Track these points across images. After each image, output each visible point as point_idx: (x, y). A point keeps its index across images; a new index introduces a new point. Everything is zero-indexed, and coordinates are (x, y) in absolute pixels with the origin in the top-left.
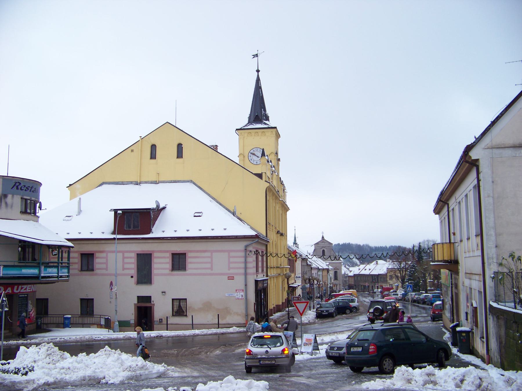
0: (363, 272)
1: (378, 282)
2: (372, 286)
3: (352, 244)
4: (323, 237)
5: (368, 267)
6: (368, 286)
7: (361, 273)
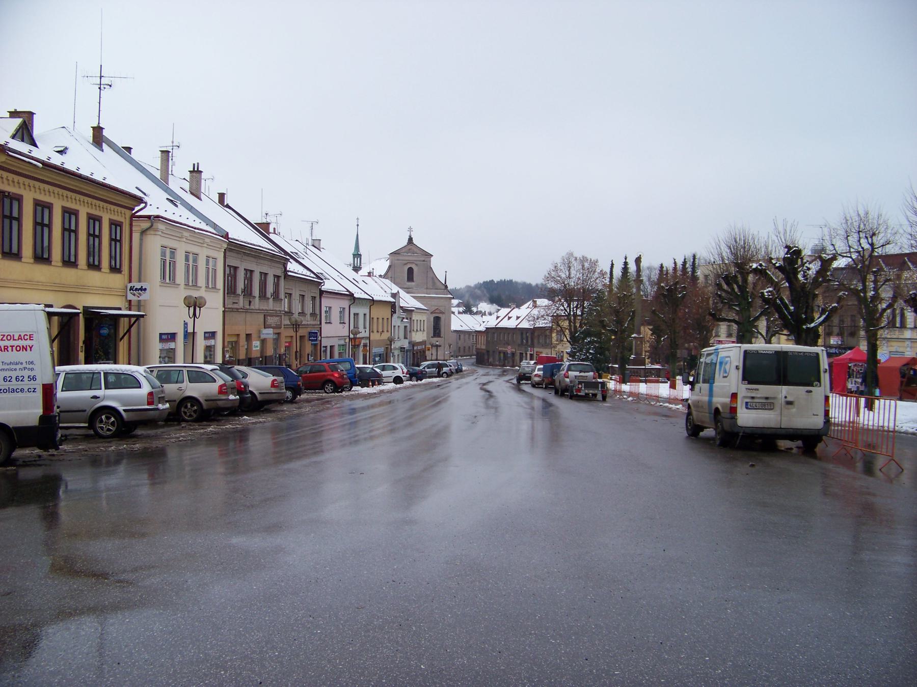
0: (505, 324)
1: (533, 346)
2: (115, 224)
3: (516, 283)
4: (410, 239)
5: (516, 312)
6: (513, 354)
7: (501, 325)
